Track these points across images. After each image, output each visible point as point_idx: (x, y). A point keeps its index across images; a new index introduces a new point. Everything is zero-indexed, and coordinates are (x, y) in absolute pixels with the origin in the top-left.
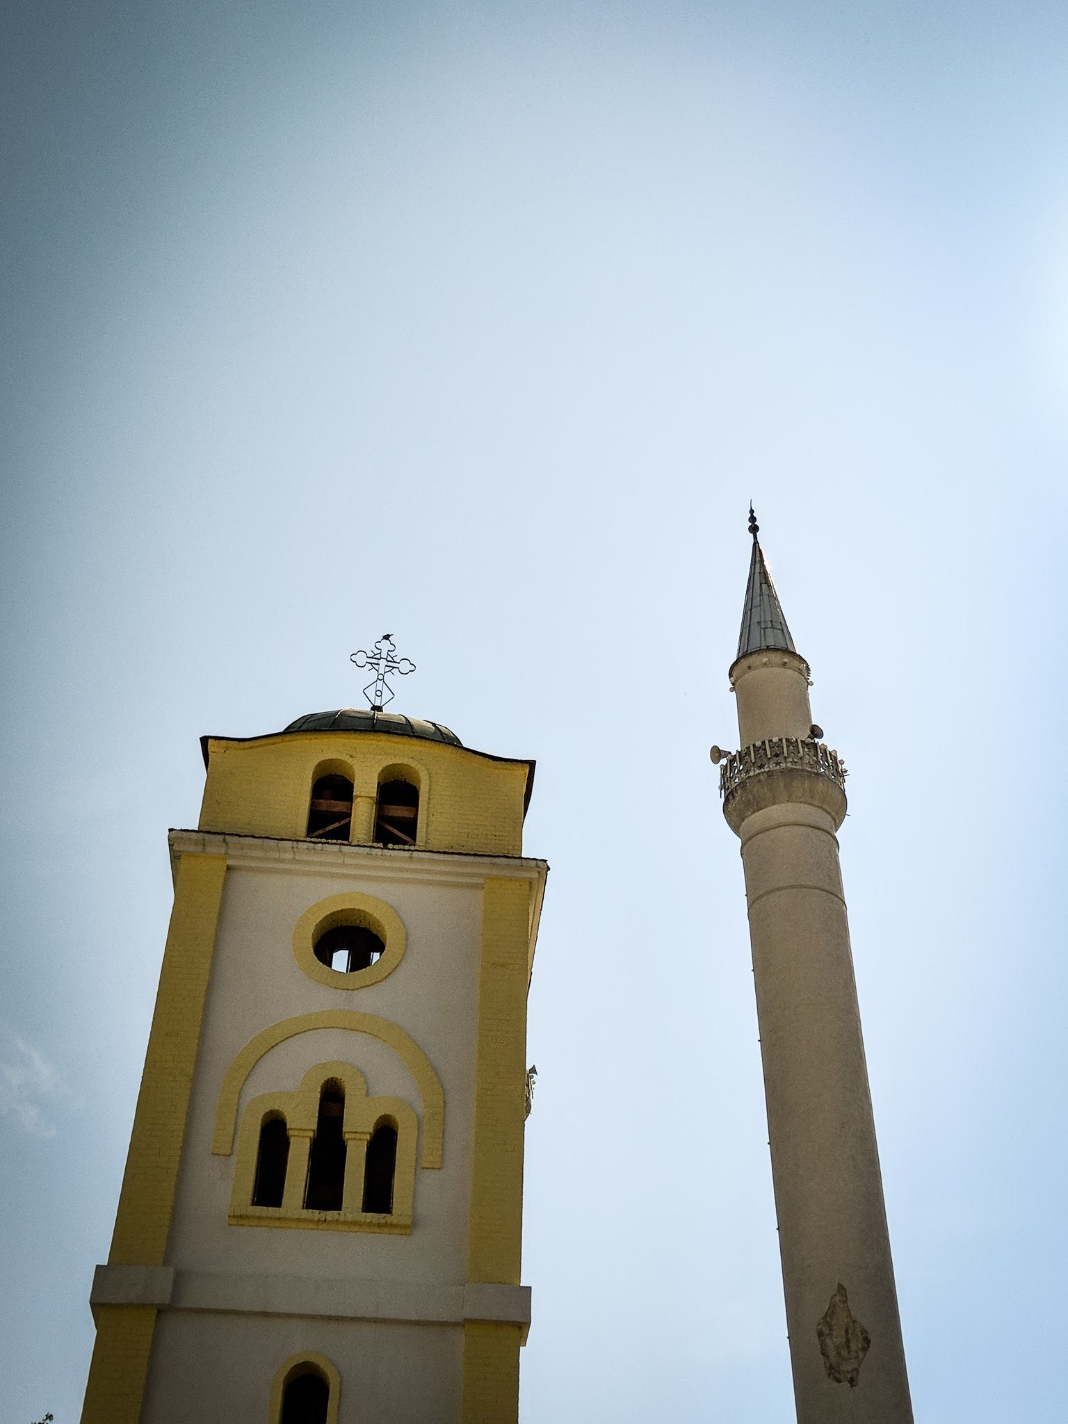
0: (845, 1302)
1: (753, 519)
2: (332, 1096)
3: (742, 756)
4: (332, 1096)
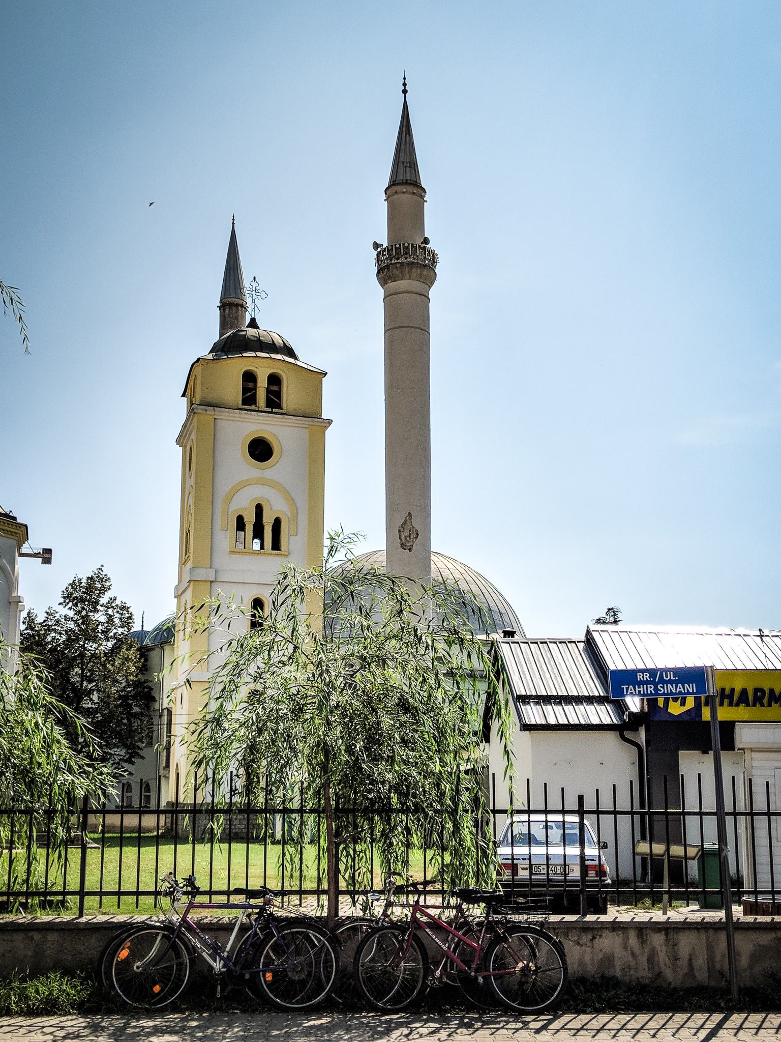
0: (411, 519)
1: (405, 84)
2: (259, 509)
3: (389, 250)
4: (259, 509)
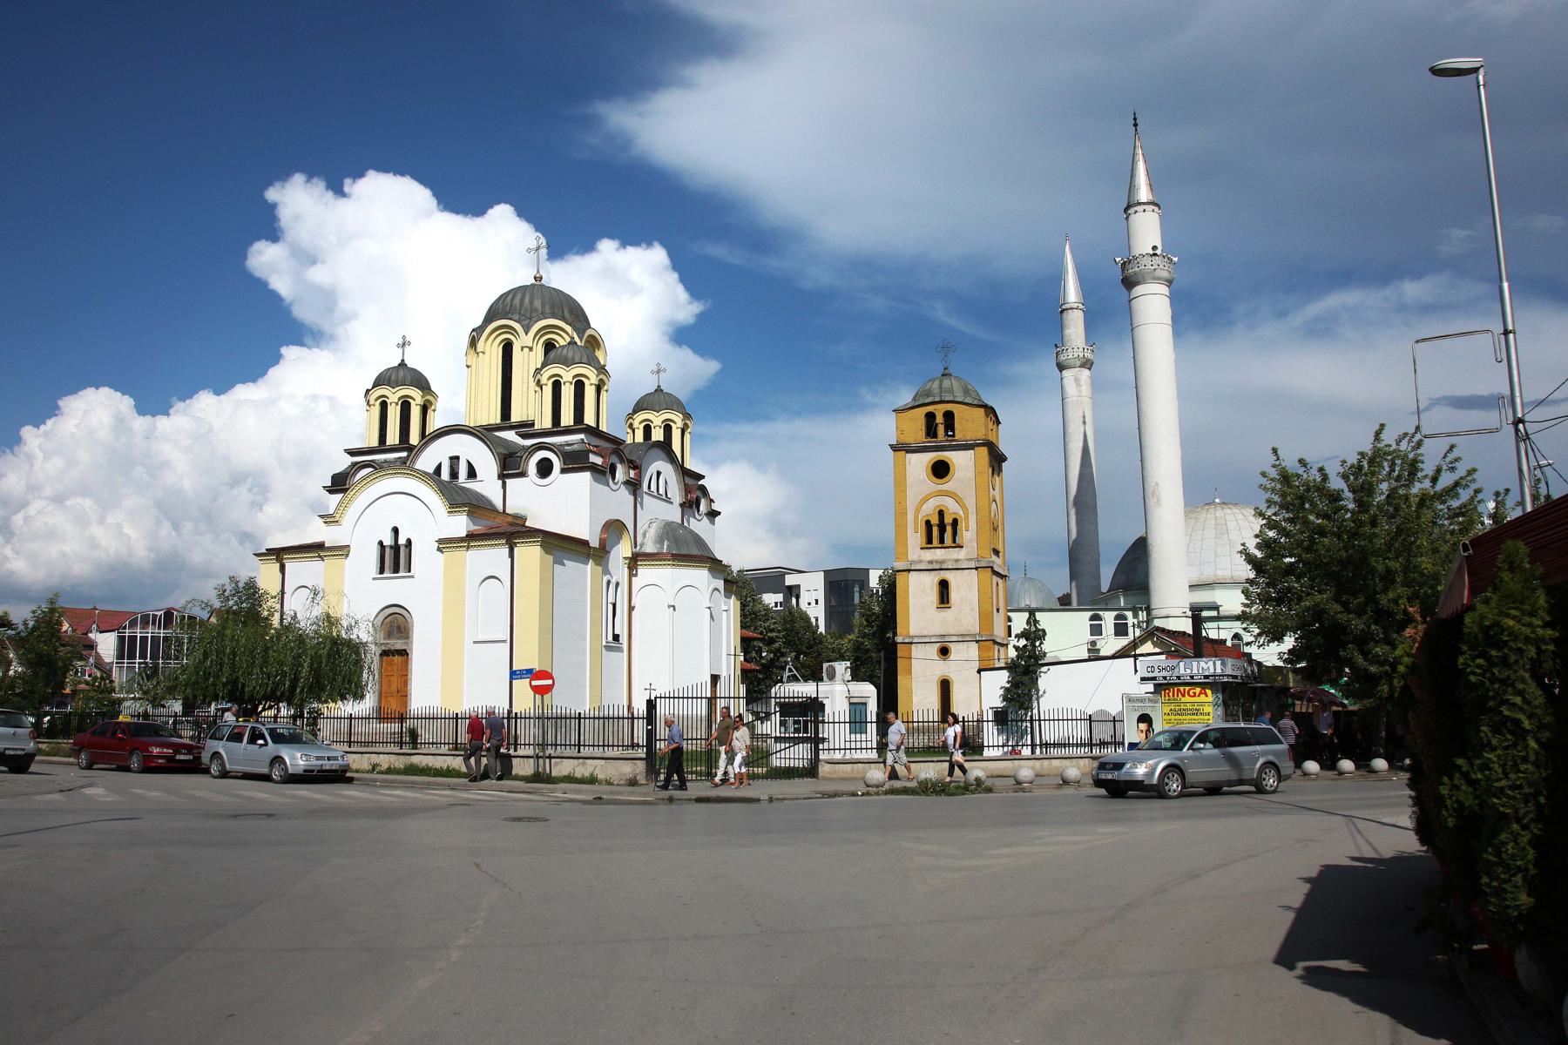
1: (1135, 119)
2: (941, 513)
4: (941, 513)
